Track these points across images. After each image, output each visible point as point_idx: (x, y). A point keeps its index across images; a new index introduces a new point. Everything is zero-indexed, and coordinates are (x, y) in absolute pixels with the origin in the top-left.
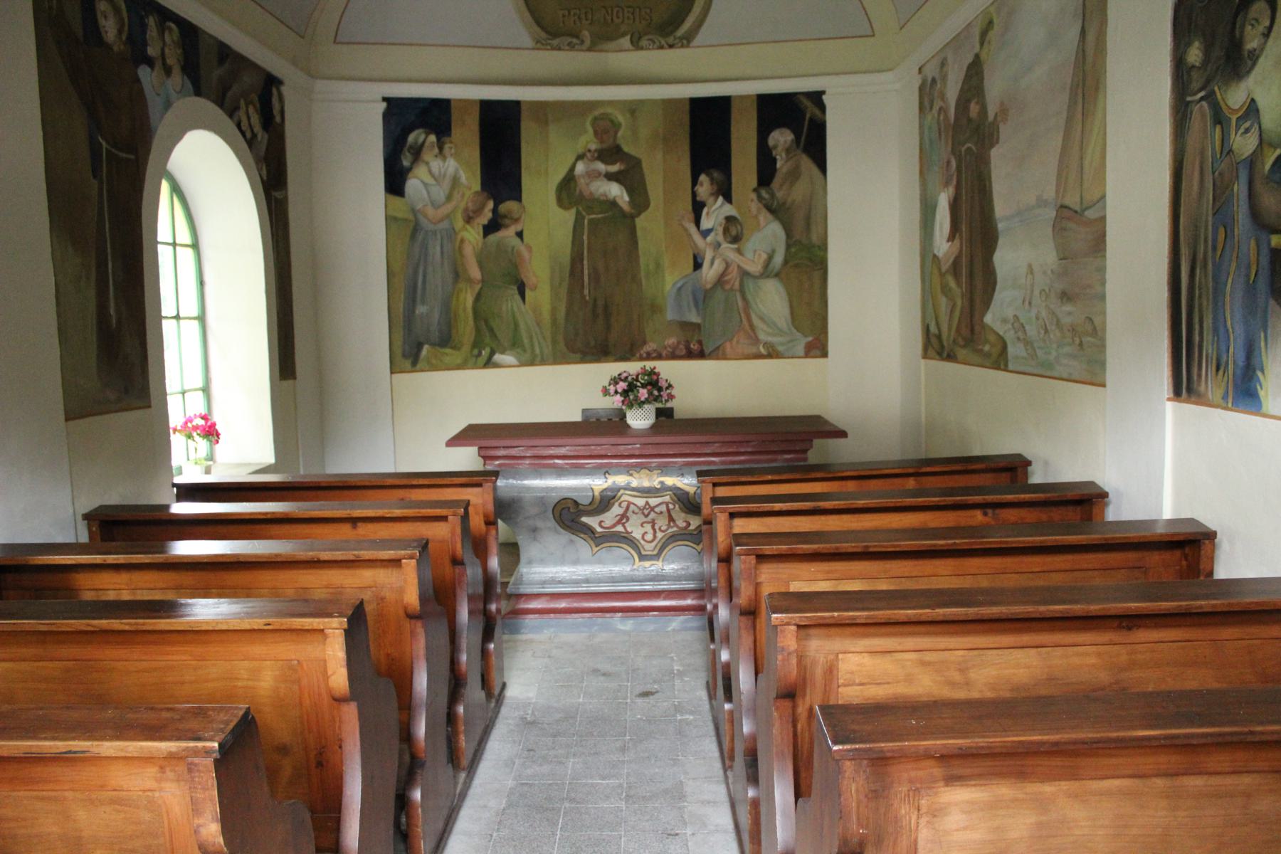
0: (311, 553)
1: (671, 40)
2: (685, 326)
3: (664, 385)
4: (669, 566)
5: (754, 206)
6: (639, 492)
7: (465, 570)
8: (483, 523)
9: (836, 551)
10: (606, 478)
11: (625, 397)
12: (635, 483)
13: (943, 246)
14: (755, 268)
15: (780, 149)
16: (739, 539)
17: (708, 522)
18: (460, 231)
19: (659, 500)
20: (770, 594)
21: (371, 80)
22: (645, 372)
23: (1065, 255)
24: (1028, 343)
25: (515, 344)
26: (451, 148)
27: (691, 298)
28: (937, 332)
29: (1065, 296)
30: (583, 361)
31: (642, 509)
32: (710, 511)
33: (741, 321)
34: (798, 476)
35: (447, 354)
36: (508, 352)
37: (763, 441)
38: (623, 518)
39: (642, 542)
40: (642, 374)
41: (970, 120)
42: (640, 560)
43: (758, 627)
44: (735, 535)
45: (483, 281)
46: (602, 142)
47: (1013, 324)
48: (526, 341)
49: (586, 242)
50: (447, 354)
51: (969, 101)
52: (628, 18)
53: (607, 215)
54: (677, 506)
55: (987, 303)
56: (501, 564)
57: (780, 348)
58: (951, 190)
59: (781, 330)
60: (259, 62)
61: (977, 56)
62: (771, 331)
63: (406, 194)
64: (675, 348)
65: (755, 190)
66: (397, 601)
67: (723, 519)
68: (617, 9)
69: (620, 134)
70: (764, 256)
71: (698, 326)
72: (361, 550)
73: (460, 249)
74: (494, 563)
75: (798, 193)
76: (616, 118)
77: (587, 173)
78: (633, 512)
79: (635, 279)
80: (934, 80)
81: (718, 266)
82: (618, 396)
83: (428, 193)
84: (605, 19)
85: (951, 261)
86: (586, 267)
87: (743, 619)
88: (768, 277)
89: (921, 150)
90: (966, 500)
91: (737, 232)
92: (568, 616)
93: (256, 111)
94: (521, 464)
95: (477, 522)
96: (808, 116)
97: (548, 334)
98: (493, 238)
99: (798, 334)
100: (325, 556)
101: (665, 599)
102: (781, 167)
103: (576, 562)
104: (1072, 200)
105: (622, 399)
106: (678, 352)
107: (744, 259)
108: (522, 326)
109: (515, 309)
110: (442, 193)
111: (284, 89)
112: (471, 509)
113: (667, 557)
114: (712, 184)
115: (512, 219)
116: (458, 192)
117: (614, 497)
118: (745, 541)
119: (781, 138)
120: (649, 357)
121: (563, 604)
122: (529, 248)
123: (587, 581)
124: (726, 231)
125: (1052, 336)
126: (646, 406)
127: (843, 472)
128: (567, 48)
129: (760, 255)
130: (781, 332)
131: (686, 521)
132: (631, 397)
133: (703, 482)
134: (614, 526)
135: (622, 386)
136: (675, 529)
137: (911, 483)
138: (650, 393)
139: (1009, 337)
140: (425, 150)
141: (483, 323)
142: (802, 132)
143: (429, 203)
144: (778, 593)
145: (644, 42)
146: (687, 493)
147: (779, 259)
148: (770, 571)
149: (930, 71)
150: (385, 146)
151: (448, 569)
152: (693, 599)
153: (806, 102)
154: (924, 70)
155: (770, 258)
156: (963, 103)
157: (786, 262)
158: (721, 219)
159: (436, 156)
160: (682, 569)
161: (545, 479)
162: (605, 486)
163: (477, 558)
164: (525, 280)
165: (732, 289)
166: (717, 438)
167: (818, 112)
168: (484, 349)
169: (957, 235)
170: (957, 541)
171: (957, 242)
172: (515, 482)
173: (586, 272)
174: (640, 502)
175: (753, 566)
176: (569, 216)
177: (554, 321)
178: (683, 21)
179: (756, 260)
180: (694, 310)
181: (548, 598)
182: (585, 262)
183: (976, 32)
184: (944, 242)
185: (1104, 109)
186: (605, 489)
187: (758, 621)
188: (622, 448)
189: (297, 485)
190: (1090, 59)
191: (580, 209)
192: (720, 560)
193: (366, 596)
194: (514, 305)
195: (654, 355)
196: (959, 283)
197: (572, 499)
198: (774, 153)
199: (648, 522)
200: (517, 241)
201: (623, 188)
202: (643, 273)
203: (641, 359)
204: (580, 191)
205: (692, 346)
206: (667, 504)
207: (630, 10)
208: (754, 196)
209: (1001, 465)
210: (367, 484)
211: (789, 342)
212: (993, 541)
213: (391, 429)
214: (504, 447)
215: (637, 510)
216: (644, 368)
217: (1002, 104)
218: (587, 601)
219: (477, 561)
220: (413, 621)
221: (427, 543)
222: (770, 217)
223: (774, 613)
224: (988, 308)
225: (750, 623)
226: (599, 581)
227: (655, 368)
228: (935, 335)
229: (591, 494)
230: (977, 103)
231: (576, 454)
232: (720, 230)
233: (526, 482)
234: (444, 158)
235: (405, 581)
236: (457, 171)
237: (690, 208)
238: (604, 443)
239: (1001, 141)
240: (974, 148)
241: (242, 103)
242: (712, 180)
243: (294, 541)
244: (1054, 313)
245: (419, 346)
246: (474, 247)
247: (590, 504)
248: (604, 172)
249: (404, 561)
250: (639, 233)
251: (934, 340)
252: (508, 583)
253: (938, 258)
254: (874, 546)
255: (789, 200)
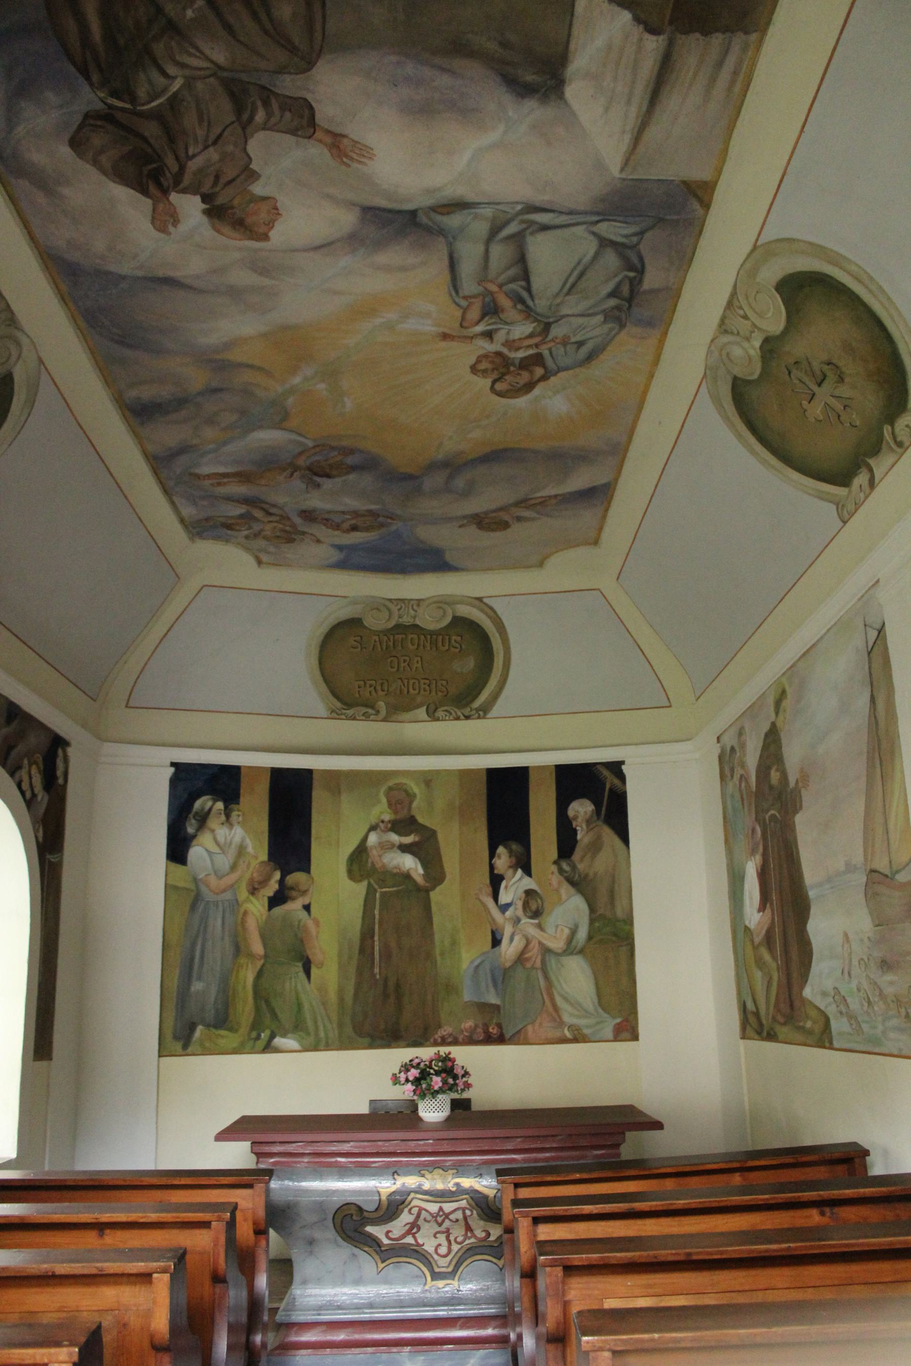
0: (45, 1266)
1: (467, 711)
2: (484, 1008)
3: (460, 1072)
4: (467, 1287)
5: (556, 879)
6: (432, 1195)
7: (228, 1289)
8: (251, 1233)
9: (655, 1260)
10: (394, 1179)
11: (417, 1086)
12: (427, 1186)
13: (754, 917)
14: (557, 945)
15: (579, 820)
16: (543, 1247)
17: (510, 1230)
18: (243, 903)
19: (454, 1205)
20: (579, 1312)
21: (164, 745)
22: (438, 1058)
23: (879, 920)
24: (851, 1017)
25: (298, 1027)
26: (239, 816)
27: (489, 975)
28: (754, 1009)
29: (886, 965)
30: (371, 1046)
31: (434, 1216)
32: (511, 1217)
33: (544, 1002)
34: (610, 1174)
35: (222, 1037)
36: (289, 1035)
37: (570, 1135)
38: (413, 1228)
39: (436, 1257)
40: (436, 1060)
41: (771, 788)
42: (432, 1280)
43: (569, 1359)
44: (539, 1242)
45: (266, 956)
46: (396, 812)
47: (834, 997)
48: (310, 1023)
49: (377, 917)
50: (222, 1037)
51: (769, 768)
52: (425, 690)
53: (400, 888)
54: (475, 1212)
55: (804, 977)
56: (270, 1283)
57: (586, 1031)
58: (758, 858)
59: (586, 1011)
60: (46, 722)
61: (773, 725)
62: (577, 1013)
63: (189, 862)
64: (473, 1030)
65: (555, 863)
66: (142, 1329)
67: (525, 1224)
68: (414, 681)
69: (415, 804)
70: (567, 932)
71: (497, 1008)
72: (106, 1261)
73: (243, 922)
74: (262, 1281)
75: (600, 865)
76: (412, 789)
77: (380, 843)
78: (425, 1220)
79: (429, 956)
80: (733, 749)
81: (518, 943)
82: (410, 1084)
83: (212, 860)
84: (401, 690)
85: (764, 932)
86: (377, 943)
87: (551, 1347)
88: (572, 954)
89: (725, 818)
90: (799, 1197)
91: (538, 908)
92: (348, 1351)
93: (40, 772)
94: (299, 1162)
95: (244, 1231)
96: (608, 787)
97: (335, 1018)
98: (278, 910)
99: (606, 1015)
100: (62, 1269)
101: (462, 1328)
102: (581, 839)
103: (358, 1281)
104: (882, 864)
105: (414, 1087)
106: (475, 1037)
107: (545, 935)
108: (306, 1006)
109: (299, 987)
110: (227, 863)
111: (70, 751)
112: (238, 1214)
113: (464, 1275)
114: (510, 857)
115: (299, 891)
116: (244, 862)
117: (403, 1202)
118: (549, 1249)
119: (581, 809)
120: (444, 1042)
121: (341, 1336)
122: (317, 923)
123: (371, 1306)
124: (526, 905)
125: (876, 1008)
126: (440, 1096)
127: (659, 1168)
128: (364, 718)
129: (562, 930)
130: (587, 1014)
131: (484, 1231)
132: (424, 1086)
133: (503, 1182)
134: (404, 1236)
135: (414, 1073)
136: (473, 1240)
137: (737, 1179)
138: (445, 1082)
139: (831, 1011)
140: (211, 816)
141: (263, 1002)
142: (602, 802)
143: (212, 872)
144: (589, 1311)
145: (440, 713)
146: (486, 1197)
147: (582, 934)
148: (580, 1286)
149: (729, 740)
150: (170, 812)
151: (207, 1288)
152: (494, 1328)
153: (606, 773)
154: (721, 739)
155: (574, 932)
156: (763, 771)
157: (590, 938)
158: (520, 893)
159: (223, 824)
160: (482, 1289)
161: (326, 1180)
162: (394, 1188)
163: (243, 1275)
164: (310, 957)
165: (533, 968)
166: (521, 1132)
167: (617, 782)
168: (263, 1032)
169: (768, 905)
170: (791, 1245)
171: (768, 911)
172: (291, 1183)
173: (377, 948)
174: (433, 1208)
175: (560, 1280)
176: (360, 889)
177: (341, 1000)
178: (479, 694)
179: (558, 935)
180: (492, 990)
181: (324, 1328)
182: (376, 938)
183: (771, 701)
184: (755, 911)
185: (902, 772)
186: (394, 1192)
187: (568, 1351)
188: (413, 1144)
189: (37, 1184)
190: (882, 723)
191: (372, 881)
192: (523, 1276)
193: (107, 1321)
194: (299, 986)
195: (450, 1040)
196: (774, 958)
197: (355, 1204)
198: (574, 824)
199: (443, 1232)
200: (303, 914)
201: (417, 860)
202: (437, 951)
203: (436, 1044)
204: (373, 863)
205: (491, 1030)
206: (464, 1210)
207: (427, 682)
208: (554, 868)
209: (836, 1155)
210: (122, 1183)
211: (598, 1023)
212: (835, 1243)
213: (155, 1120)
214: (280, 1142)
215: (429, 1218)
216: (438, 1054)
217: (802, 770)
218: (370, 1331)
219: (243, 1280)
220: (160, 1355)
221: (184, 1253)
222: (572, 890)
223: (585, 1334)
224: (806, 981)
225: (559, 1354)
226: (384, 1306)
227: (450, 1053)
228: (753, 1013)
229: (377, 1198)
230: (777, 770)
231: (361, 1150)
232: (520, 904)
233: (304, 1184)
234: (231, 826)
235: (155, 1302)
236: (243, 840)
237: (488, 881)
238: (393, 1139)
239: (804, 809)
240: (777, 815)
241: (26, 762)
242: (511, 852)
243: (28, 1250)
244: (876, 983)
245: (192, 1027)
246: (257, 920)
247: (377, 1209)
248: (397, 843)
249: (155, 1275)
250: (434, 908)
251: (750, 1017)
252: (279, 1308)
253: (750, 930)
254: (699, 1253)
255: (591, 874)
